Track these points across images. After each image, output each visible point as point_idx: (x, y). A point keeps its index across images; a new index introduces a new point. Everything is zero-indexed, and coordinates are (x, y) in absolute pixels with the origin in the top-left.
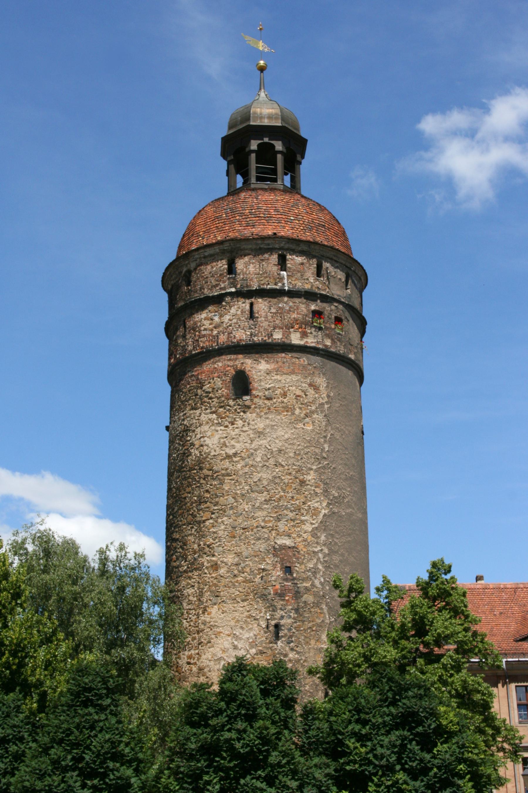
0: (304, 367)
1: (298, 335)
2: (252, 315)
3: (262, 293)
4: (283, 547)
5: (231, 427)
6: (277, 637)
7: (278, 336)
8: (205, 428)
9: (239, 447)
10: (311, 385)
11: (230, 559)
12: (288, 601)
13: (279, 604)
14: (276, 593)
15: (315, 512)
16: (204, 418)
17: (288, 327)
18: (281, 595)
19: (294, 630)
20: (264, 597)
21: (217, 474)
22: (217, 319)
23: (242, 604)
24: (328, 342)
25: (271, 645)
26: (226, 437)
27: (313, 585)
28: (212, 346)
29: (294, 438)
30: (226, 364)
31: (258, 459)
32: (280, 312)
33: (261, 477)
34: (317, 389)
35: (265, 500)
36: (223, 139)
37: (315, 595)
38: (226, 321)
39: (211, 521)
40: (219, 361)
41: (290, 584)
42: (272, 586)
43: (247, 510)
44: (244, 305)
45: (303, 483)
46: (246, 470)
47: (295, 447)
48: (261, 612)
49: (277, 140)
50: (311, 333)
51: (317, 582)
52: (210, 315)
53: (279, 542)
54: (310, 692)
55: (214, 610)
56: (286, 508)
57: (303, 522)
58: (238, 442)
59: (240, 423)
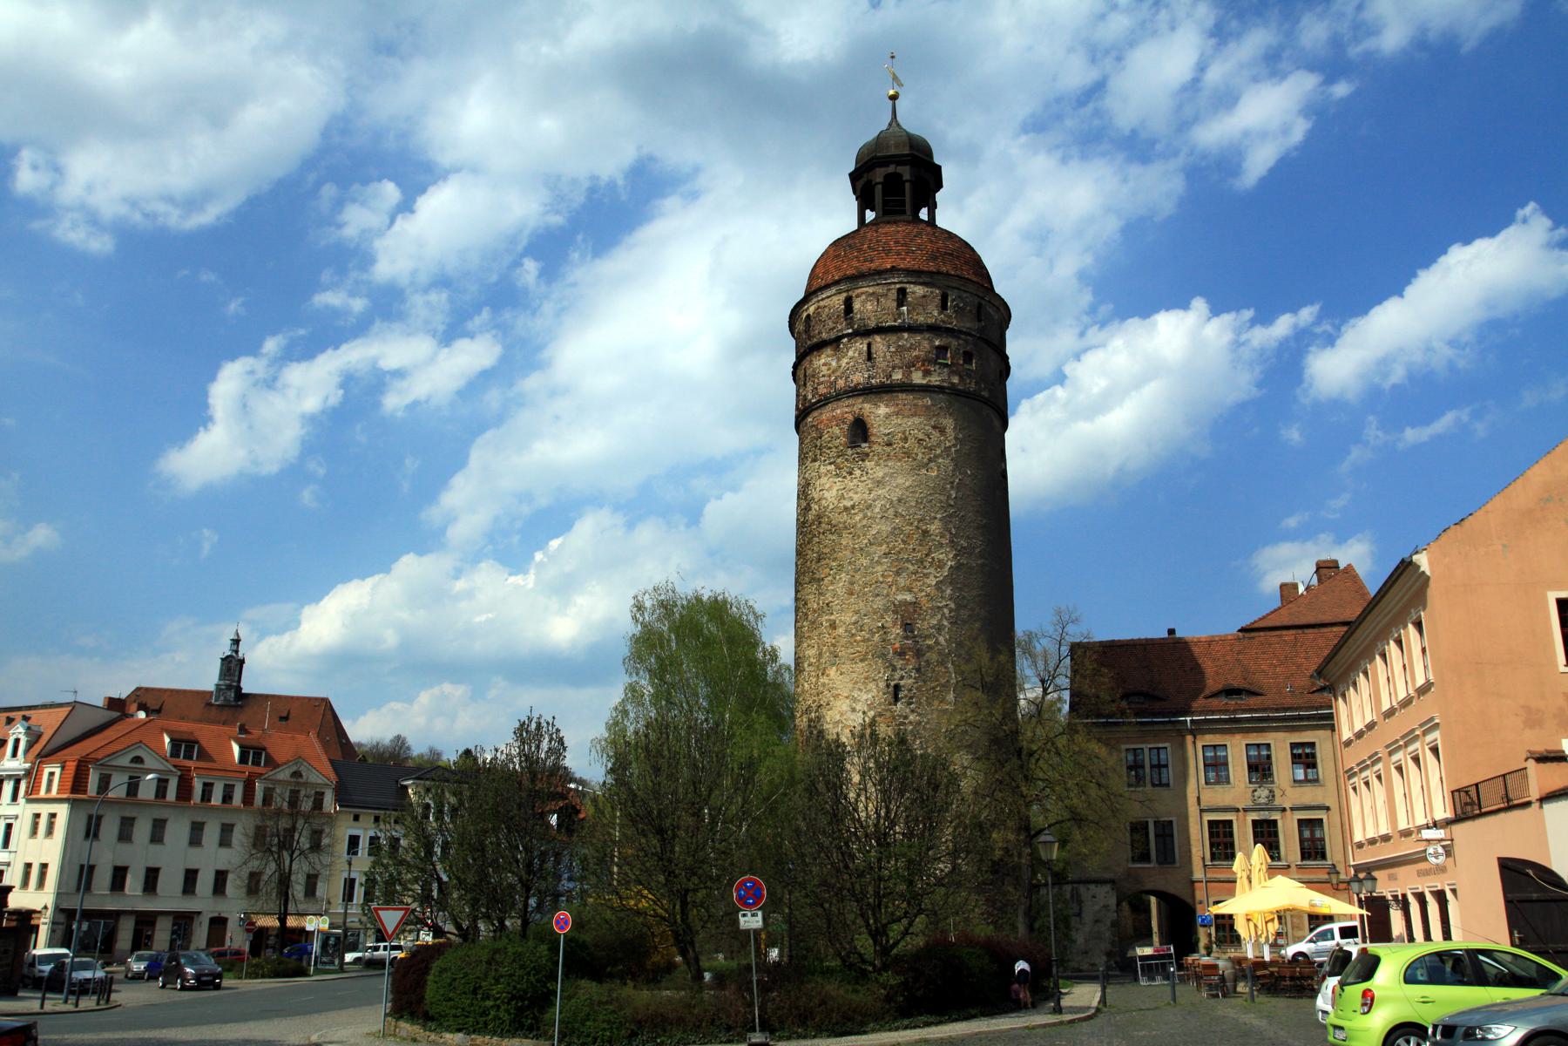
0: (927, 408)
1: (920, 374)
2: (870, 357)
3: (879, 330)
4: (905, 603)
6: (896, 699)
7: (898, 376)
8: (824, 480)
9: (856, 498)
10: (934, 427)
11: (849, 618)
13: (899, 664)
14: (895, 653)
15: (941, 565)
16: (823, 469)
17: (909, 367)
18: (901, 654)
20: (883, 656)
22: (834, 364)
24: (956, 380)
27: (937, 643)
30: (844, 410)
34: (942, 431)
36: (851, 175)
37: (940, 653)
44: (861, 345)
45: (925, 532)
51: (941, 639)
53: (900, 597)
55: (832, 672)
56: (908, 561)
57: (926, 576)
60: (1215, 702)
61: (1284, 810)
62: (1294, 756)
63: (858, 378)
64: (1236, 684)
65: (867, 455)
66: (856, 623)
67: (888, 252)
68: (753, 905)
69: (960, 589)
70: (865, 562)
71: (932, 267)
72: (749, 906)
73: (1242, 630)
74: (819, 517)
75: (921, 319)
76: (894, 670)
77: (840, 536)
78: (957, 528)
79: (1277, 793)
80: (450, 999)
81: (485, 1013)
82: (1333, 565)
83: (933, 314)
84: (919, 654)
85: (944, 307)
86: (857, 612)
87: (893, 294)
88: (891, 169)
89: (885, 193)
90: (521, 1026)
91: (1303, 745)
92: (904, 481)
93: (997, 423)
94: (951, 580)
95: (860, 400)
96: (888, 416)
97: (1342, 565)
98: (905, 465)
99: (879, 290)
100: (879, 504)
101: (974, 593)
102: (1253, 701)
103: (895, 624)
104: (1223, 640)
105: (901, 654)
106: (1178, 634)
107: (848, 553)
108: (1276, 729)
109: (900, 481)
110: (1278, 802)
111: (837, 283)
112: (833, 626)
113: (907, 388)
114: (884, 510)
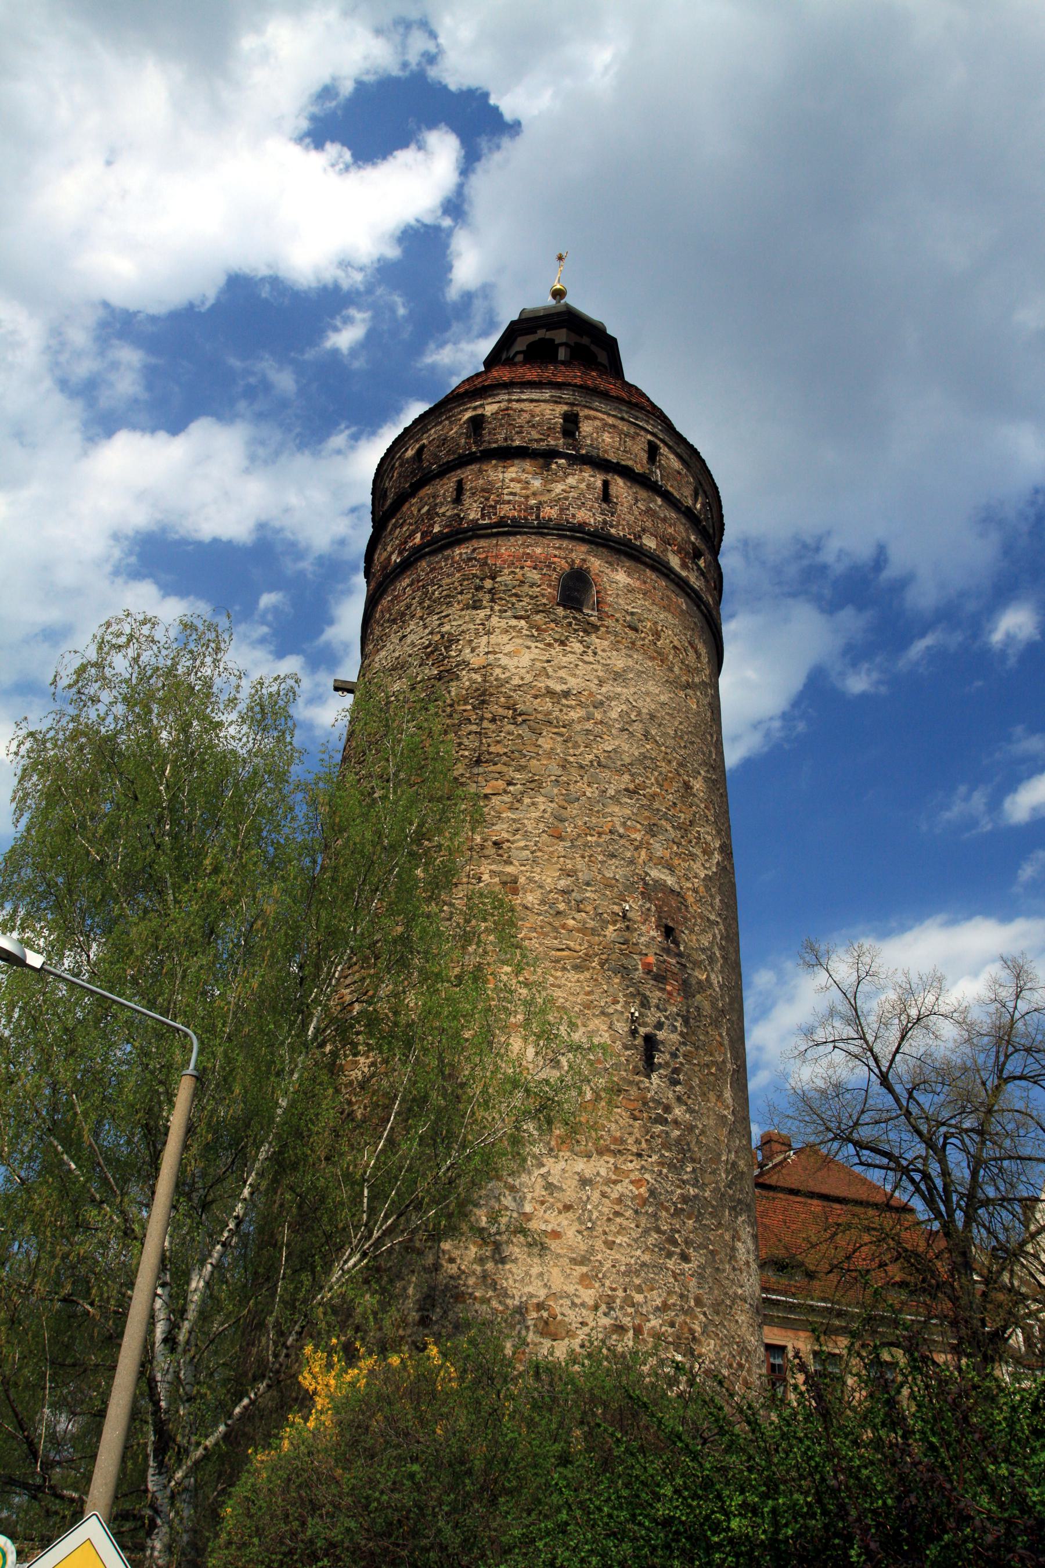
4: (660, 885)
5: (558, 648)
6: (650, 1066)
7: (650, 543)
9: (573, 683)
11: (550, 878)
12: (670, 993)
13: (655, 996)
19: (681, 1059)
20: (624, 971)
21: (524, 717)
23: (573, 976)
25: (637, 1078)
26: (548, 661)
28: (526, 519)
31: (614, 715)
33: (619, 746)
35: (626, 790)
38: (558, 491)
39: (507, 798)
40: (537, 545)
41: (673, 961)
42: (640, 954)
43: (588, 794)
46: (589, 725)
48: (616, 1002)
49: (257, 602)
52: (524, 476)
53: (654, 873)
54: (713, 1207)
58: (574, 675)
59: (578, 647)
74: (482, 697)
76: (645, 1004)
84: (687, 989)
88: (585, 341)
96: (630, 590)
99: (624, 427)
113: (658, 565)
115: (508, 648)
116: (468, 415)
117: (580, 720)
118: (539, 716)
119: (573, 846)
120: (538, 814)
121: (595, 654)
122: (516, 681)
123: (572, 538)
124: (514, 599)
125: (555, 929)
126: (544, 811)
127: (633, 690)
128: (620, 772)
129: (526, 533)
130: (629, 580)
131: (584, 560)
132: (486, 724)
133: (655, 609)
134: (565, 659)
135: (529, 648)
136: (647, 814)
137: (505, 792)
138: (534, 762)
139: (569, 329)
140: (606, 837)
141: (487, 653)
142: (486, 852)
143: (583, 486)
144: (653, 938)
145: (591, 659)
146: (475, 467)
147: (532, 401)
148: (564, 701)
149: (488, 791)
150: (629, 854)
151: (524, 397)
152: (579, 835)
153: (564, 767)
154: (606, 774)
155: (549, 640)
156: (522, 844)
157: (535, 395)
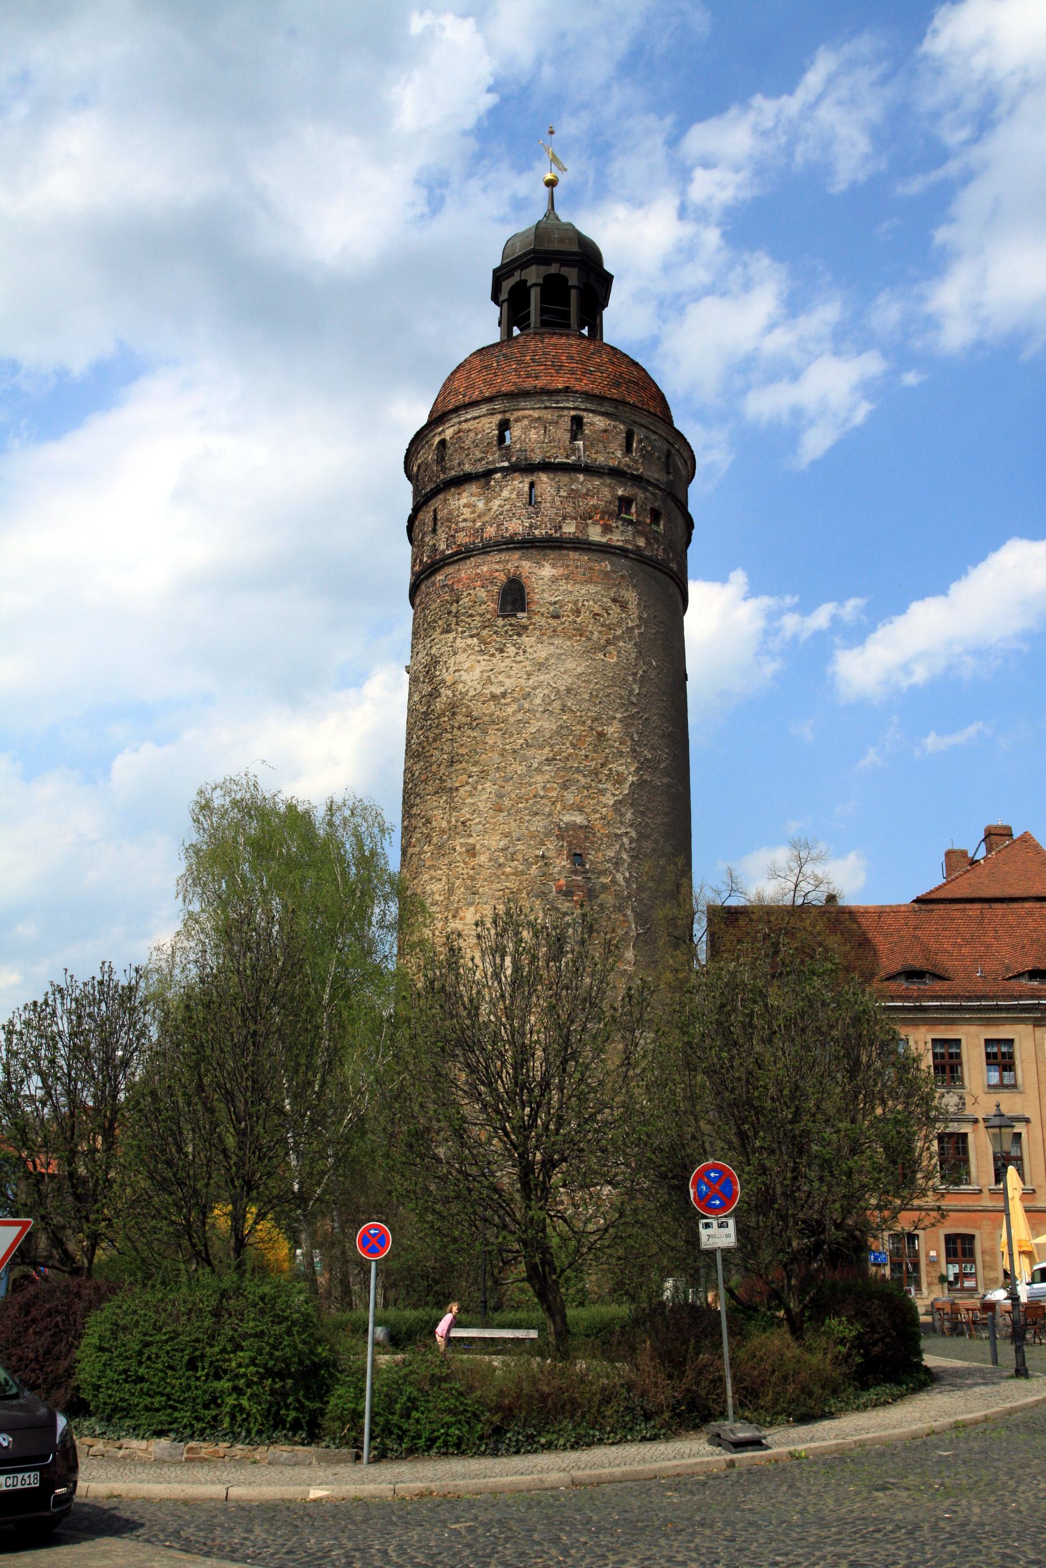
0: (606, 574)
1: (598, 529)
3: (546, 467)
4: (573, 826)
5: (498, 656)
7: (570, 528)
8: (461, 657)
9: (509, 683)
10: (614, 600)
11: (495, 842)
13: (565, 906)
14: (559, 891)
15: (619, 780)
16: (460, 643)
17: (586, 517)
18: (567, 893)
20: (543, 895)
22: (481, 505)
24: (641, 542)
27: (614, 881)
28: (474, 543)
29: (591, 674)
30: (495, 567)
31: (538, 701)
32: (573, 495)
34: (624, 606)
35: (547, 760)
38: (495, 508)
39: (468, 788)
43: (519, 772)
44: (520, 484)
45: (601, 735)
46: (520, 716)
47: (592, 686)
50: (617, 527)
51: (619, 877)
53: (567, 818)
56: (578, 771)
57: (602, 792)
58: (509, 677)
59: (511, 650)
60: (893, 986)
61: (976, 1121)
62: (988, 1055)
63: (516, 527)
64: (919, 964)
65: (526, 628)
66: (504, 849)
67: (559, 368)
68: (723, 1207)
69: (643, 813)
70: (521, 769)
71: (614, 393)
72: (714, 1210)
73: (918, 901)
74: (453, 708)
75: (601, 459)
77: (485, 732)
78: (640, 734)
79: (969, 1100)
80: (141, 1379)
81: (214, 1401)
82: (1006, 833)
83: (615, 455)
85: (628, 449)
86: (506, 835)
87: (566, 423)
88: (554, 269)
89: (544, 299)
90: (279, 1423)
91: (998, 1042)
92: (576, 666)
93: (681, 607)
94: (632, 800)
95: (517, 555)
96: (554, 580)
97: (1016, 835)
98: (577, 645)
99: (548, 415)
100: (540, 693)
101: (658, 820)
102: (939, 986)
103: (559, 854)
104: (894, 911)
105: (567, 893)
106: (841, 902)
107: (496, 757)
108: (969, 1021)
109: (570, 664)
110: (969, 1111)
111: (489, 400)
112: (472, 852)
113: (581, 545)
114: (547, 701)
115: (466, 666)
116: (437, 439)
117: (514, 713)
118: (486, 719)
119: (509, 814)
120: (487, 796)
121: (525, 652)
122: (472, 693)
123: (508, 549)
124: (469, 620)
125: (498, 877)
126: (490, 793)
127: (553, 674)
128: (541, 747)
129: (476, 555)
130: (554, 571)
131: (517, 567)
132: (456, 732)
133: (578, 587)
134: (504, 664)
135: (479, 662)
136: (562, 773)
137: (468, 783)
138: (484, 756)
139: (538, 264)
140: (531, 802)
141: (455, 671)
142: (458, 830)
143: (514, 496)
144: (564, 867)
145: (521, 658)
146: (441, 496)
147: (475, 418)
148: (503, 701)
149: (457, 785)
150: (547, 810)
151: (469, 417)
152: (513, 805)
153: (502, 755)
154: (531, 752)
155: (493, 651)
156: (477, 820)
157: (476, 413)
